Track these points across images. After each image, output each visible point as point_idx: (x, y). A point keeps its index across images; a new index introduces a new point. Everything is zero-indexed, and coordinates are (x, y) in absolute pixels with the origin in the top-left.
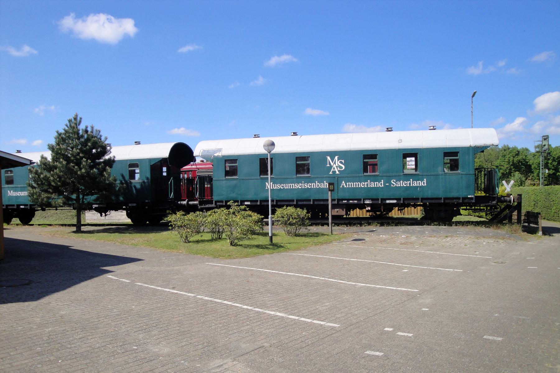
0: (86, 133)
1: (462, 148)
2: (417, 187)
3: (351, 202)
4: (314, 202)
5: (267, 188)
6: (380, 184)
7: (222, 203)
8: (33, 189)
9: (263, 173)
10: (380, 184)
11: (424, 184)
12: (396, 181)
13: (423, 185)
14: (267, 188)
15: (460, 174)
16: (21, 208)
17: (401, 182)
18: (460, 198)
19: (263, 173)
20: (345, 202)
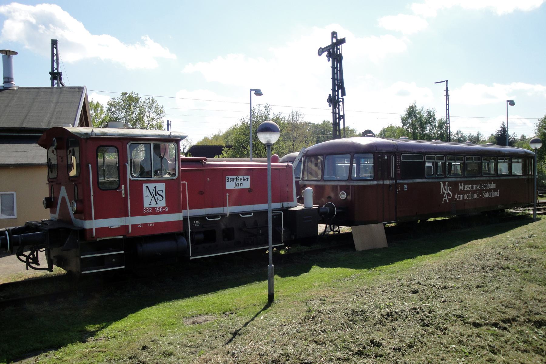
14: (441, 193)
17: (488, 193)
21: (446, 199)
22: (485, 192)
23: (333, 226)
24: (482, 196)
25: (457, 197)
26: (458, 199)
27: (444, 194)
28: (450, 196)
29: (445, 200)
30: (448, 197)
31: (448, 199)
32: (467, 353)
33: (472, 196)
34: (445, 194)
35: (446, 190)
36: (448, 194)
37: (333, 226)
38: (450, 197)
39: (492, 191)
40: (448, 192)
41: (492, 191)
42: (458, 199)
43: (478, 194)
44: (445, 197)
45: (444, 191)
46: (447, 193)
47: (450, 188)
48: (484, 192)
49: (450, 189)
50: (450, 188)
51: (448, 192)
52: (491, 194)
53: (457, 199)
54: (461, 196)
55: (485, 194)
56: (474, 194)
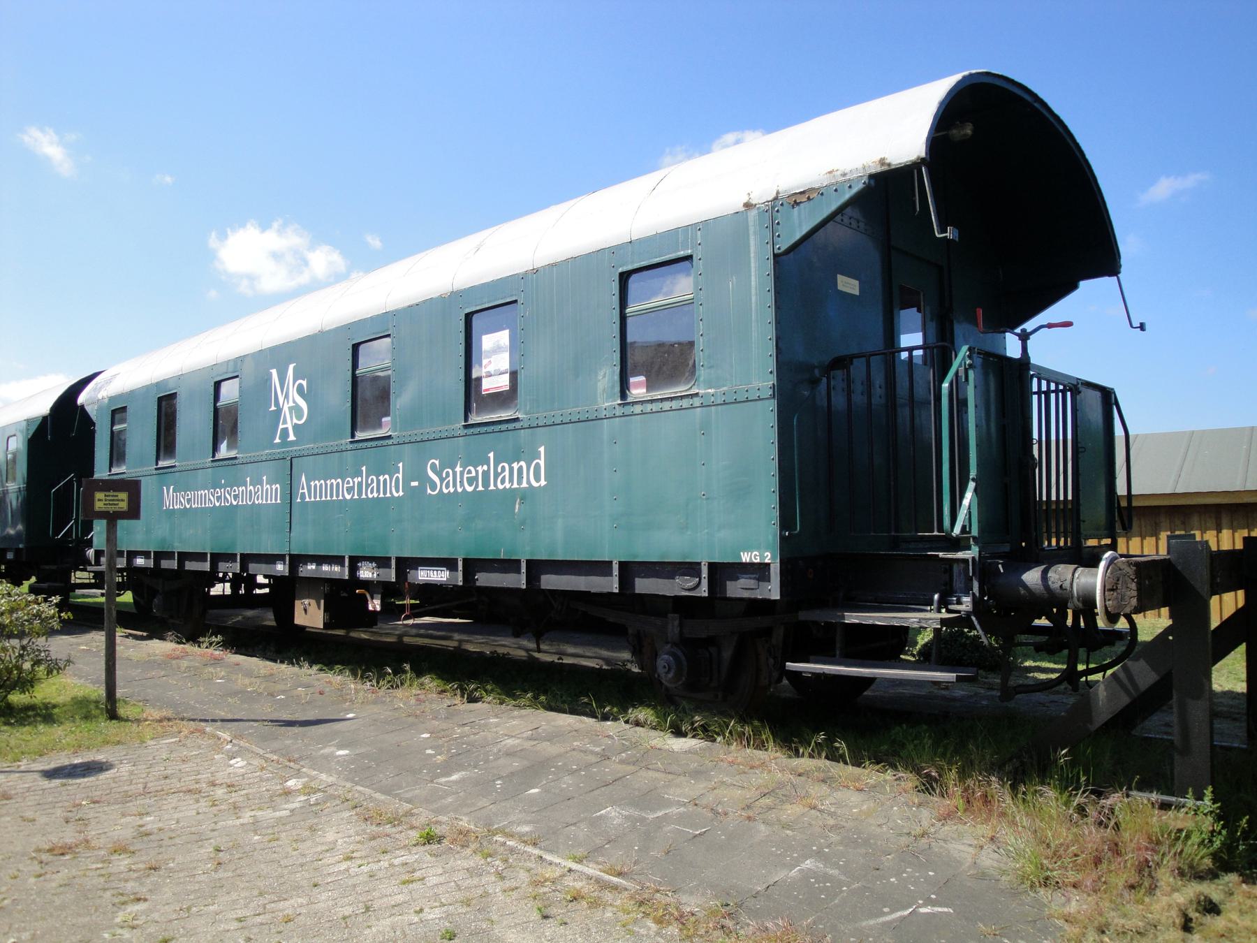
0: (215, 785)
1: (704, 226)
2: (510, 495)
3: (326, 572)
4: (406, 575)
5: (273, 408)
6: (390, 486)
7: (337, 569)
8: (243, 618)
9: (229, 230)
10: (390, 486)
11: (537, 479)
12: (443, 467)
13: (535, 484)
14: (273, 408)
15: (697, 402)
16: (1072, 543)
17: (458, 469)
18: (518, 561)
19: (229, 230)
20: (331, 572)
21: (287, 428)
22: (443, 467)
23: (99, 495)
24: (422, 488)
25: (306, 491)
26: (310, 498)
27: (279, 411)
28: (299, 417)
29: (285, 431)
30: (295, 421)
31: (296, 427)
32: (1209, 891)
33: (368, 486)
34: (286, 409)
35: (287, 397)
36: (296, 410)
37: (99, 495)
38: (299, 418)
39: (491, 455)
40: (294, 402)
41: (491, 455)
42: (310, 498)
43: (400, 476)
44: (285, 422)
45: (281, 399)
46: (291, 404)
47: (300, 386)
48: (433, 465)
49: (300, 390)
50: (300, 386)
51: (294, 402)
52: (486, 474)
53: (307, 499)
54: (321, 485)
55: (439, 474)
56: (381, 478)
